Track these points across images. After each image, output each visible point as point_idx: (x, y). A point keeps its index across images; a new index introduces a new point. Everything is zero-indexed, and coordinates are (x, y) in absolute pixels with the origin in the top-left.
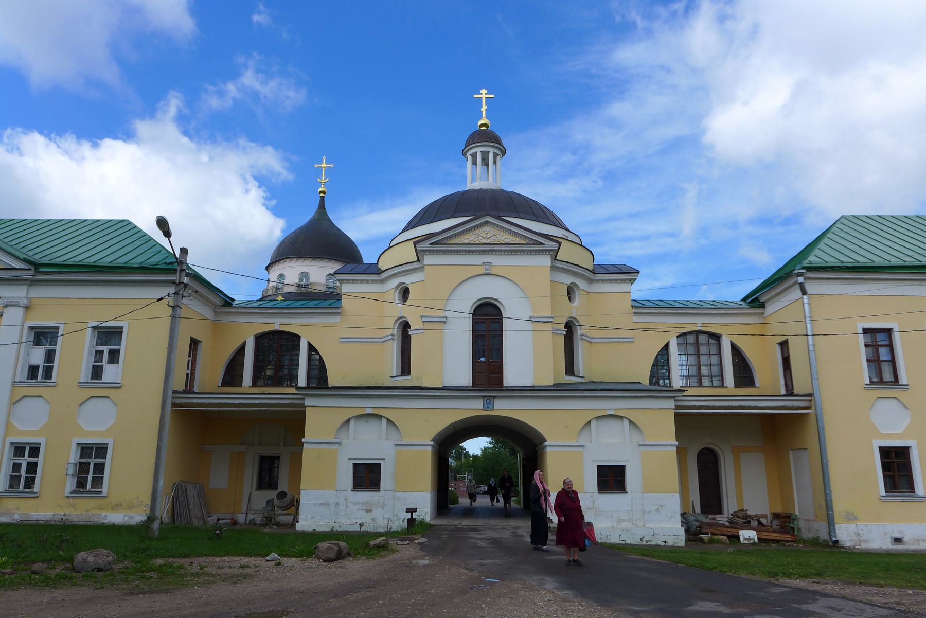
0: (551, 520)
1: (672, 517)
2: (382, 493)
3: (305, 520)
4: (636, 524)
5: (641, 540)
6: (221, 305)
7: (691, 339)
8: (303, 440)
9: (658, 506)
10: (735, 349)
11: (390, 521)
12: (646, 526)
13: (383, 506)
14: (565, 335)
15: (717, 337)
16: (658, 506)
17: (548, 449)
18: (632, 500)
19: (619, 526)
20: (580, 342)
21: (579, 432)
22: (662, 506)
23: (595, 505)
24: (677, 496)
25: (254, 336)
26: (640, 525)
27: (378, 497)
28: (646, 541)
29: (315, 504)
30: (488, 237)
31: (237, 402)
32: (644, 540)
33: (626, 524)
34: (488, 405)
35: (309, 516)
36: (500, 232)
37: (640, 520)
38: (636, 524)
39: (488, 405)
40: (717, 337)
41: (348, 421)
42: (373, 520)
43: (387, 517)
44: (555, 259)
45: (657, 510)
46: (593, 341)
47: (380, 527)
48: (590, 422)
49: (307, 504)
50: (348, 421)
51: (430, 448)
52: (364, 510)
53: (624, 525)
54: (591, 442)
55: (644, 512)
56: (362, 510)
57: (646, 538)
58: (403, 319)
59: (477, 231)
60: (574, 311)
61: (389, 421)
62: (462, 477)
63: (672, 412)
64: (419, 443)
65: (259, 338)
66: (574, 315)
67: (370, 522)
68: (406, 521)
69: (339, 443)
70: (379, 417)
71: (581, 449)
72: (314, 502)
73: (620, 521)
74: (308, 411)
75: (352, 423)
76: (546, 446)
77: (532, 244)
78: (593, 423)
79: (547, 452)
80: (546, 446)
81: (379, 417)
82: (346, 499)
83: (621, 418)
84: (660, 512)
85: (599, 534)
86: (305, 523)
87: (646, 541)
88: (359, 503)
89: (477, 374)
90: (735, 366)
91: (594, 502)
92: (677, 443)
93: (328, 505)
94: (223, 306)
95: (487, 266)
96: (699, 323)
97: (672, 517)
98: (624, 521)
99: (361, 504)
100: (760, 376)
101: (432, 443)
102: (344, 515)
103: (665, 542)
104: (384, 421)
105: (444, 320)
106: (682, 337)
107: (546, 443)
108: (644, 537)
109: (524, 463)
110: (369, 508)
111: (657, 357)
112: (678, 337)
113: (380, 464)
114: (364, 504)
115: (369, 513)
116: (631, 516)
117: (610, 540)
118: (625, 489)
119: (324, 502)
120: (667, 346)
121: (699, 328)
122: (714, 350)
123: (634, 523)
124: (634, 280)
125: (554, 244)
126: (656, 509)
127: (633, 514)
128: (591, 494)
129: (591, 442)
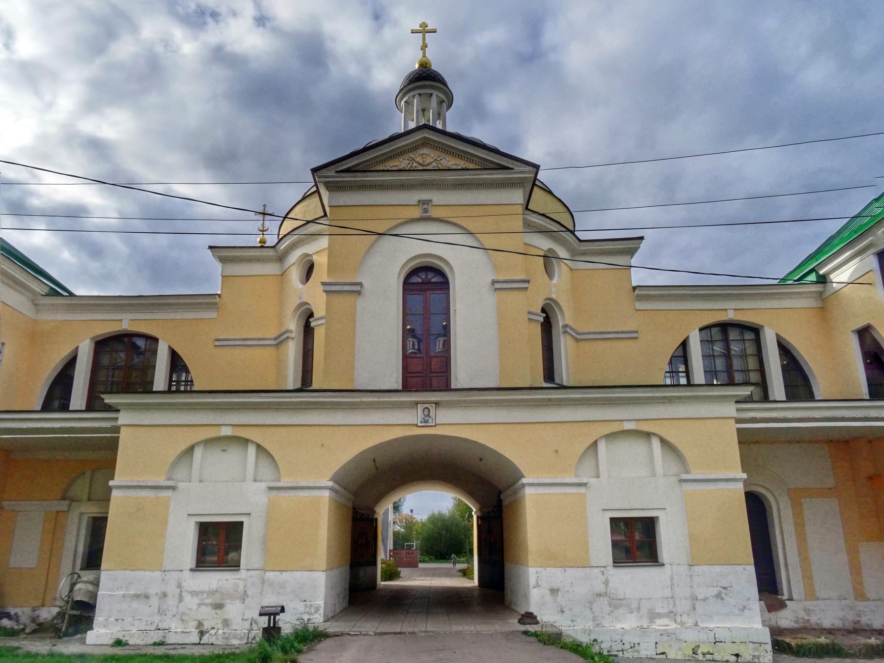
0: (536, 617)
1: (744, 607)
2: (242, 573)
3: (105, 626)
4: (681, 621)
5: (695, 652)
6: (43, 293)
7: (716, 333)
8: (111, 483)
9: (719, 589)
10: (785, 350)
11: (254, 624)
12: (701, 625)
13: (244, 597)
14: (542, 324)
15: (756, 331)
16: (719, 589)
17: (528, 491)
18: (672, 579)
19: (654, 626)
20: (562, 337)
21: (580, 459)
22: (725, 588)
23: (608, 589)
24: (752, 569)
25: (92, 339)
26: (690, 622)
27: (236, 581)
28: (704, 654)
29: (124, 596)
30: (426, 163)
31: (25, 425)
32: (700, 651)
33: (665, 621)
34: (426, 419)
35: (112, 619)
36: (444, 155)
37: (688, 615)
38: (681, 621)
39: (426, 419)
40: (756, 331)
41: (191, 449)
42: (226, 623)
43: (250, 617)
44: (527, 208)
45: (719, 596)
46: (579, 337)
47: (235, 637)
48: (595, 443)
49: (110, 595)
50: (191, 449)
51: (327, 494)
52: (211, 604)
53: (661, 624)
54: (598, 477)
55: (694, 598)
56: (206, 605)
57: (703, 649)
58: (308, 307)
59: (411, 155)
60: (554, 290)
61: (259, 447)
62: (409, 545)
63: (733, 426)
64: (309, 485)
65: (102, 345)
66: (554, 296)
67: (220, 626)
68: (261, 629)
69: (173, 488)
70: (245, 442)
71: (582, 490)
72: (122, 593)
73: (653, 616)
74: (124, 436)
75: (198, 453)
76: (524, 485)
77: (492, 169)
78: (602, 446)
79: (524, 495)
80: (524, 485)
81: (245, 442)
82: (179, 586)
83: (648, 435)
84: (722, 599)
85: (619, 641)
86: (102, 631)
87: (704, 654)
88: (202, 592)
89: (410, 375)
90: (785, 369)
91: (606, 583)
92: (745, 476)
93: (147, 597)
94: (47, 295)
95: (425, 206)
96: (731, 311)
97: (744, 607)
98: (660, 616)
99: (205, 595)
100: (821, 386)
101: (331, 484)
102: (174, 616)
103: (737, 655)
104: (252, 450)
105: (357, 288)
106: (705, 331)
107: (524, 481)
108: (698, 646)
109: (480, 523)
110: (218, 602)
111: (671, 359)
112: (701, 330)
113: (241, 524)
114: (212, 593)
115: (218, 611)
116: (671, 606)
117: (638, 652)
118: (657, 558)
119: (139, 593)
120: (684, 345)
121: (731, 316)
122: (750, 349)
123: (679, 619)
124: (636, 249)
125: (528, 168)
126: (715, 593)
127: (675, 604)
128: (603, 569)
129: (598, 477)
